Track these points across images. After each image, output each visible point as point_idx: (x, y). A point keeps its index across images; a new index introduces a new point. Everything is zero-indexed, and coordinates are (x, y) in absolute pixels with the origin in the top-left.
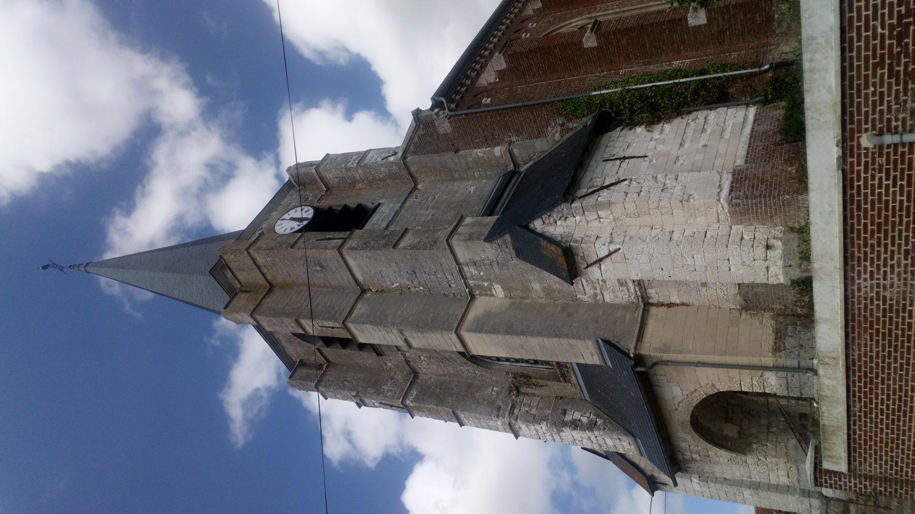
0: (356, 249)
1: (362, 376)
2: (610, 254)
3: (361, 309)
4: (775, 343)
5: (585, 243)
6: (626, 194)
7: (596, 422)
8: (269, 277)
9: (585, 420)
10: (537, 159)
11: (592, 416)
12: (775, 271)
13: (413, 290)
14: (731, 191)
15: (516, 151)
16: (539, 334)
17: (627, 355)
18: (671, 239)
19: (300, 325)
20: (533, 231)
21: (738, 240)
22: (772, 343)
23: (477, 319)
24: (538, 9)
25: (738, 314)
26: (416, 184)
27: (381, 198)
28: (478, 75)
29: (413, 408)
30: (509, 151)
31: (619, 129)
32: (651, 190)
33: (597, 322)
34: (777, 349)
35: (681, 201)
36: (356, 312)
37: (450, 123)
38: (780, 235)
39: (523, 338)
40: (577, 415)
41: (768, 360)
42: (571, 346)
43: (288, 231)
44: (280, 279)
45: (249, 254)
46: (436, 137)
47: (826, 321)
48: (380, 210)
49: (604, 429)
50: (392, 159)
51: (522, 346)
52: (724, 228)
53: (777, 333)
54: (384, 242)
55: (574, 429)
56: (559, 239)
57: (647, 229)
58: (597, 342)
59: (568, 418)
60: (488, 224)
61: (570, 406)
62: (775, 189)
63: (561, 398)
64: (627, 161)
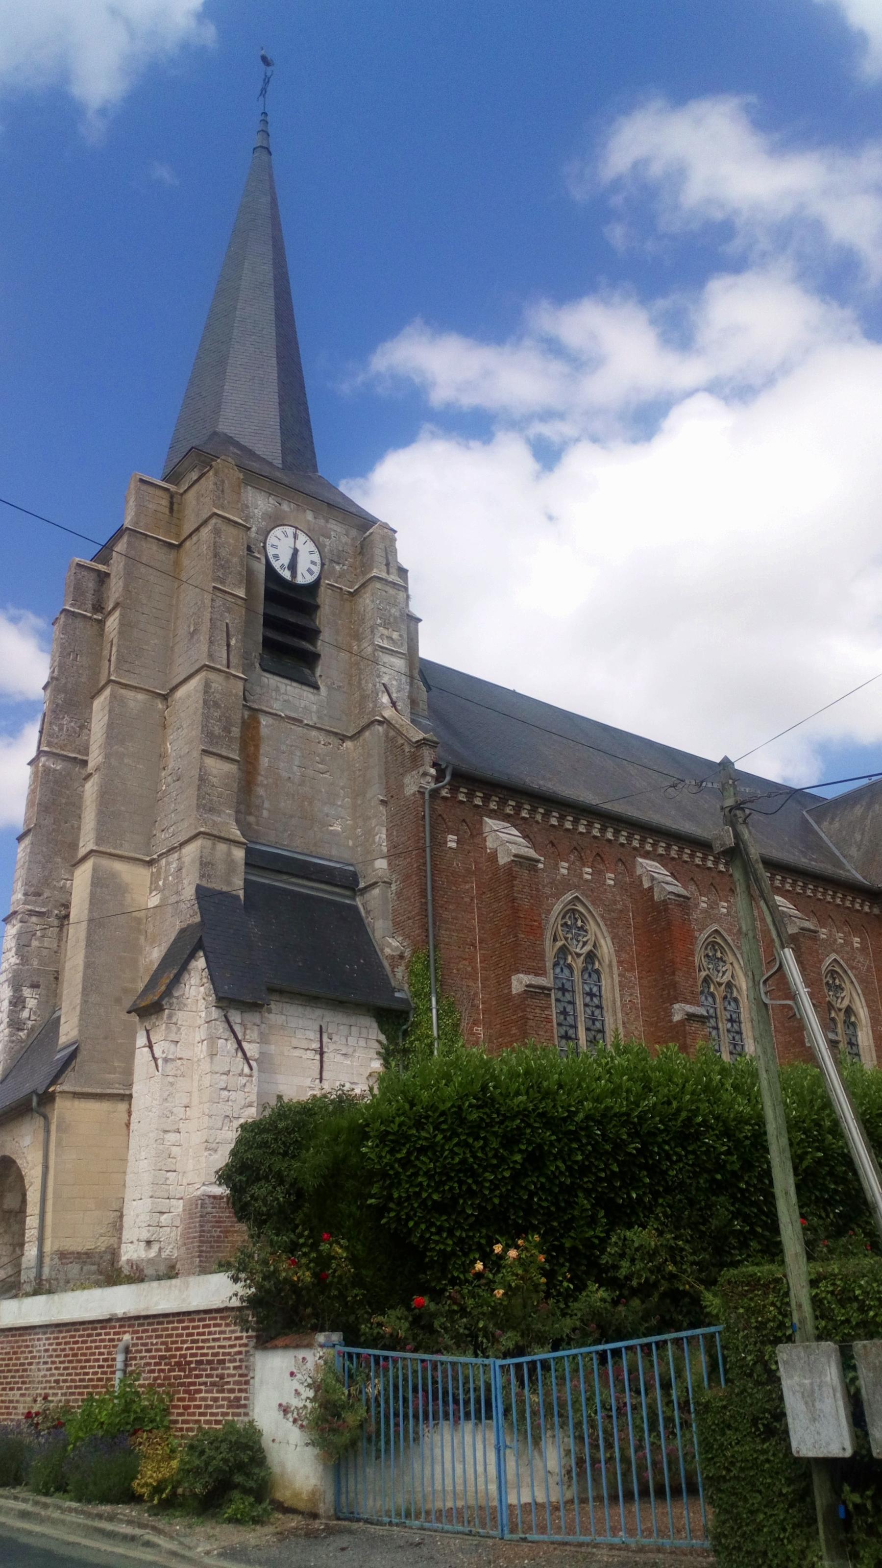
0: (206, 692)
1: (83, 679)
2: (155, 1059)
3: (135, 700)
4: (72, 1253)
5: (167, 1028)
6: (227, 1073)
7: (23, 1030)
8: (188, 544)
9: (25, 1014)
10: (366, 922)
11: (30, 1023)
12: (131, 1253)
13: (163, 774)
14: (215, 1197)
15: (376, 892)
16: (88, 965)
17: (54, 1082)
18: (166, 1131)
19: (114, 608)
20: (192, 956)
21: (159, 1209)
22: (72, 1249)
23: (114, 875)
24: (641, 881)
25: (115, 1208)
26: (351, 738)
27: (330, 688)
28: (506, 818)
29: (37, 766)
30: (376, 883)
31: (382, 1038)
32: (230, 1103)
33: (106, 1038)
34: (63, 1255)
35: (206, 1141)
36: (130, 694)
37: (414, 794)
38: (164, 1255)
39: (83, 944)
40: (31, 1003)
41: (48, 1248)
42: (74, 1008)
43: (271, 552)
44: (186, 562)
45: (210, 517)
46: (401, 771)
47: (20, 1308)
48: (306, 693)
49: (13, 1042)
50: (385, 699)
51: (77, 941)
52: (180, 1191)
53: (86, 1253)
54: (217, 731)
55: (10, 1003)
56: (176, 994)
57: (185, 1101)
58: (75, 1043)
59: (27, 992)
60: (229, 883)
61: (44, 992)
62: (211, 1247)
63: (57, 978)
64: (318, 1057)
